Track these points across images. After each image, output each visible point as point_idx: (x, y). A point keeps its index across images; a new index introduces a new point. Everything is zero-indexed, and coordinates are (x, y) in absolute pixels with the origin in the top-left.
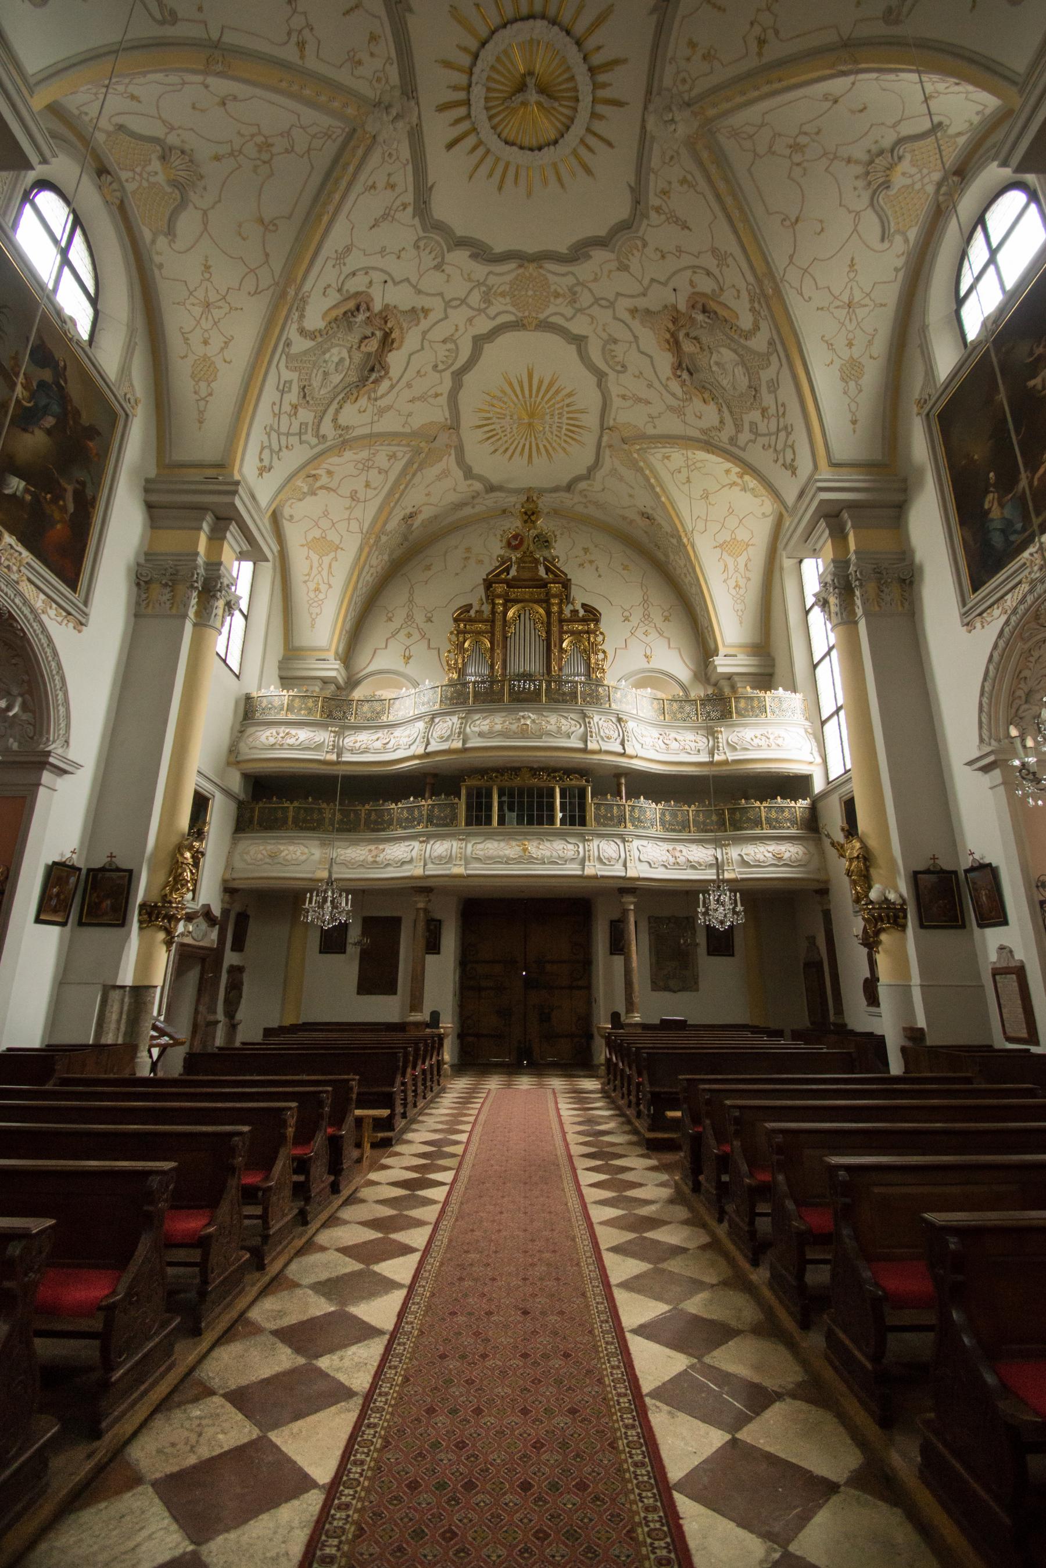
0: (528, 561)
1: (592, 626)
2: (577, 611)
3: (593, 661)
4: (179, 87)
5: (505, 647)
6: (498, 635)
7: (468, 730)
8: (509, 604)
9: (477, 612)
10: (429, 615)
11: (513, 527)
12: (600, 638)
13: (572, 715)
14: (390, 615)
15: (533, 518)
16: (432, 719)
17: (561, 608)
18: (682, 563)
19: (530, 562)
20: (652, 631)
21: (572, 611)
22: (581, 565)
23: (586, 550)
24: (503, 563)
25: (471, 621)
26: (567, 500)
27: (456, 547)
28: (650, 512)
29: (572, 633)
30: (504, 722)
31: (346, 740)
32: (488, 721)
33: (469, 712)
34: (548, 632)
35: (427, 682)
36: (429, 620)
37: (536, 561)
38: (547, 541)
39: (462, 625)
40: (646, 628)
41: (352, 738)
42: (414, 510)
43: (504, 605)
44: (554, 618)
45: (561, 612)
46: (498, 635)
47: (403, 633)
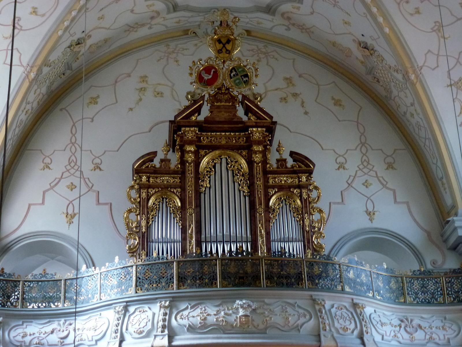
0: (223, 98)
1: (304, 179)
2: (285, 160)
3: (307, 223)
4: (304, 75)
5: (198, 205)
6: (190, 191)
7: (174, 322)
8: (202, 152)
9: (162, 161)
10: (97, 161)
11: (204, 58)
12: (314, 194)
13: (299, 302)
14: (47, 160)
15: (229, 47)
16: (126, 309)
17: (265, 157)
18: (409, 101)
19: (226, 101)
20: (373, 181)
21: (278, 161)
22: (284, 100)
23: (289, 81)
24: (195, 102)
25: (155, 172)
26: (266, 22)
27: (129, 76)
28: (369, 42)
29: (280, 188)
30: (218, 312)
31: (13, 334)
32: (198, 311)
33: (174, 300)
34: (251, 186)
35: (117, 259)
36: (97, 167)
37: (233, 99)
38: (246, 76)
39: (144, 178)
40: (366, 177)
41: (20, 331)
42: (83, 35)
43: (196, 153)
44: (258, 169)
45: (265, 162)
46: (190, 191)
47: (65, 182)
